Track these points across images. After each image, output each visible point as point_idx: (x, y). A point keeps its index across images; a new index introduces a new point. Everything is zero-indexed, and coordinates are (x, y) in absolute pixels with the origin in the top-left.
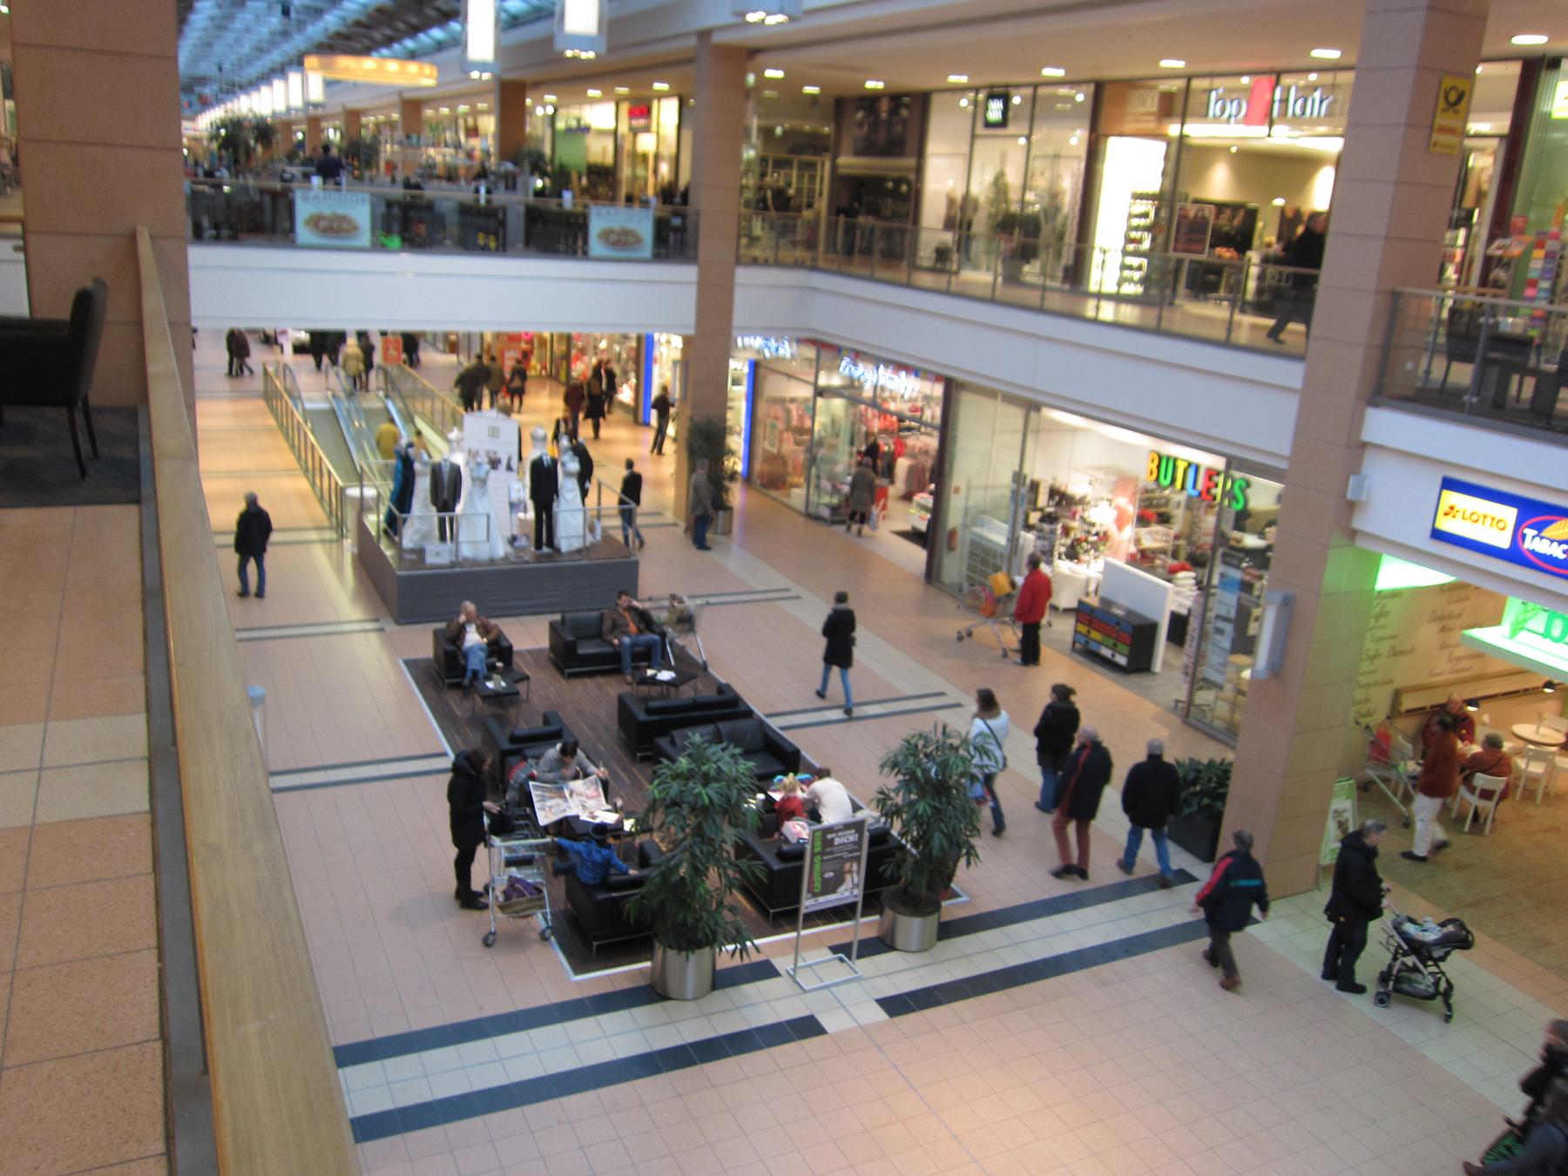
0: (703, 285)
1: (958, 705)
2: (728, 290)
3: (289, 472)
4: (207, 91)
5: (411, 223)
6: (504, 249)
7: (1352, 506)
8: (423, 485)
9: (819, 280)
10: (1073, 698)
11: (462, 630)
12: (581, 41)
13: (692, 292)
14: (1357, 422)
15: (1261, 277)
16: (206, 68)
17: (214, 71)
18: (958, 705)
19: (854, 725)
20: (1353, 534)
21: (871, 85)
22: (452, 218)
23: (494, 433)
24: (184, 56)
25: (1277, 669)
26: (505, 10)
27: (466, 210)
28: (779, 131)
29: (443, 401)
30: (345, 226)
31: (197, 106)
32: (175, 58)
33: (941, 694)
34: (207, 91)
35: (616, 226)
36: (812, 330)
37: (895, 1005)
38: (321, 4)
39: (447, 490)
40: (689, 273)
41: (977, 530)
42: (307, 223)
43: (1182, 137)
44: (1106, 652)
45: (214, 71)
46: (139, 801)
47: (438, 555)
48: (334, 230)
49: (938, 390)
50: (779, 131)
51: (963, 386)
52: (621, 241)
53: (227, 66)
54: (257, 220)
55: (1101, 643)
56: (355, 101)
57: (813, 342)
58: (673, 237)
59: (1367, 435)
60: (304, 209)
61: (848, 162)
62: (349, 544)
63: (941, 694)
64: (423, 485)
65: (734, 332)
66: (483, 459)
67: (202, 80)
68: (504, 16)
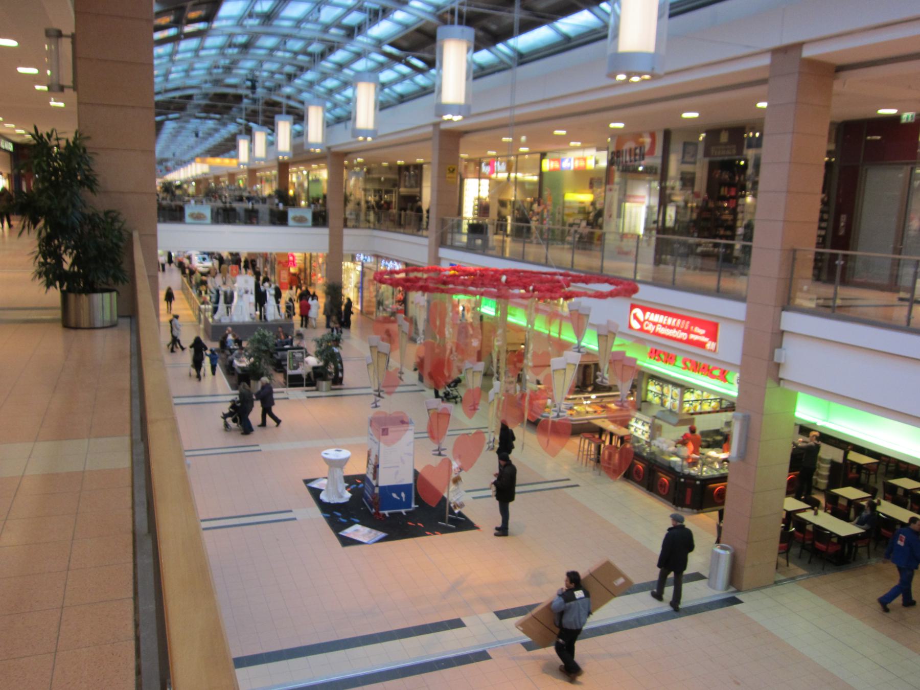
0: (331, 235)
1: (577, 486)
2: (340, 237)
3: (186, 309)
4: (169, 164)
5: (225, 216)
7: (778, 365)
8: (222, 298)
11: (226, 336)
12: (316, 145)
14: (778, 321)
15: (512, 226)
16: (168, 155)
17: (171, 156)
19: (680, 623)
20: (779, 380)
21: (399, 162)
22: (242, 213)
23: (246, 282)
24: (159, 148)
25: (743, 455)
26: (474, 62)
27: (247, 211)
28: (382, 179)
31: (164, 172)
32: (153, 152)
33: (568, 480)
34: (169, 164)
37: (308, 397)
38: (389, 4)
39: (229, 299)
40: (325, 231)
43: (516, 178)
45: (171, 156)
46: (124, 462)
47: (225, 320)
48: (198, 217)
50: (382, 179)
52: (300, 220)
53: (177, 154)
54: (173, 212)
56: (218, 173)
58: (320, 219)
59: (783, 327)
60: (188, 211)
61: (403, 190)
62: (202, 326)
63: (568, 480)
64: (222, 298)
66: (243, 291)
67: (166, 160)
68: (474, 67)
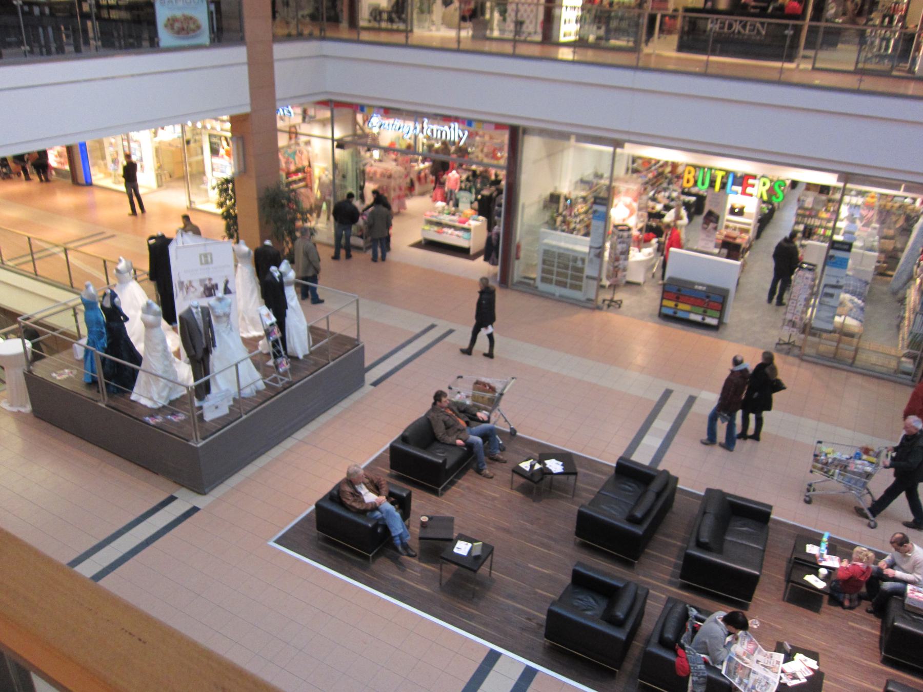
0: (252, 63)
1: (451, 331)
2: (269, 65)
6: (220, 41)
9: (329, 47)
10: (127, 325)
13: (244, 71)
18: (451, 331)
29: (482, 151)
30: (192, 26)
33: (433, 326)
35: (178, 14)
36: (326, 93)
40: (239, 54)
41: (546, 241)
42: (166, 26)
44: (698, 318)
49: (505, 137)
51: (525, 131)
55: (690, 312)
57: (325, 103)
63: (433, 326)
65: (278, 104)
